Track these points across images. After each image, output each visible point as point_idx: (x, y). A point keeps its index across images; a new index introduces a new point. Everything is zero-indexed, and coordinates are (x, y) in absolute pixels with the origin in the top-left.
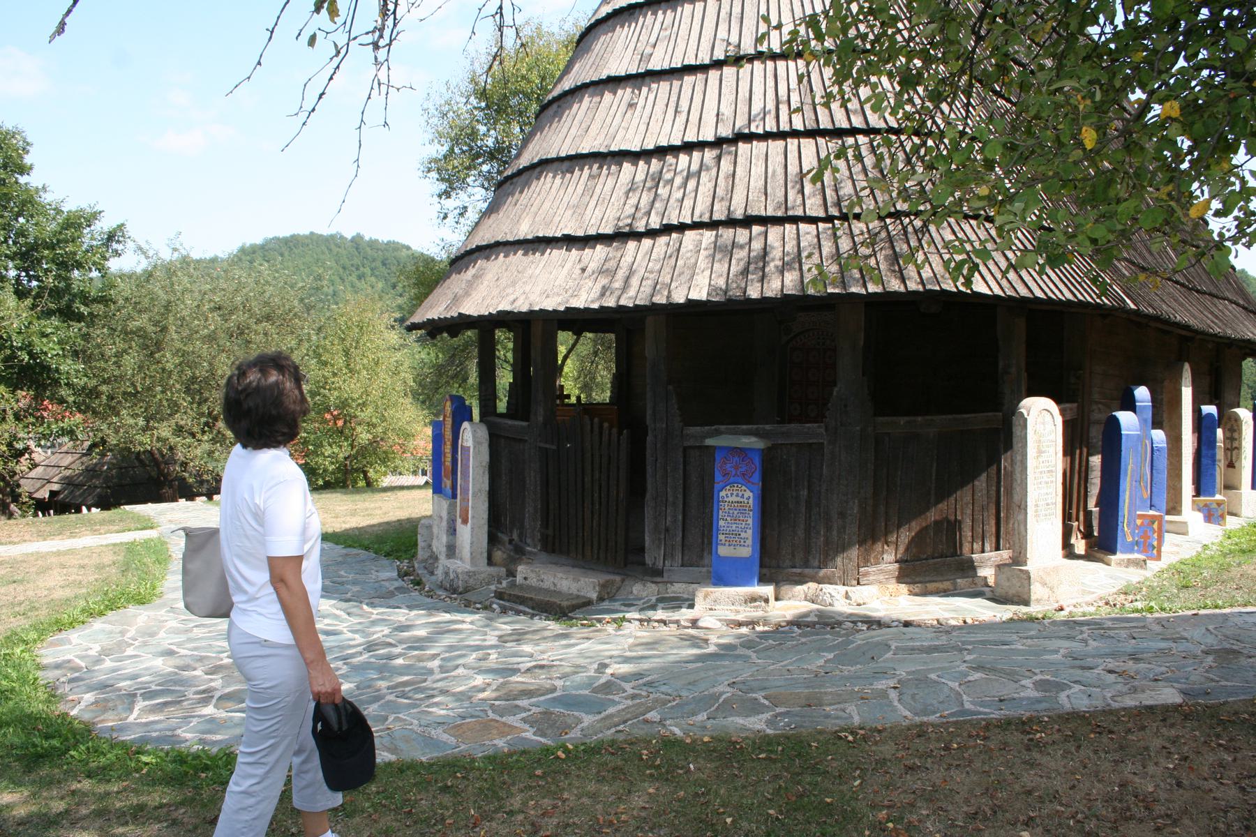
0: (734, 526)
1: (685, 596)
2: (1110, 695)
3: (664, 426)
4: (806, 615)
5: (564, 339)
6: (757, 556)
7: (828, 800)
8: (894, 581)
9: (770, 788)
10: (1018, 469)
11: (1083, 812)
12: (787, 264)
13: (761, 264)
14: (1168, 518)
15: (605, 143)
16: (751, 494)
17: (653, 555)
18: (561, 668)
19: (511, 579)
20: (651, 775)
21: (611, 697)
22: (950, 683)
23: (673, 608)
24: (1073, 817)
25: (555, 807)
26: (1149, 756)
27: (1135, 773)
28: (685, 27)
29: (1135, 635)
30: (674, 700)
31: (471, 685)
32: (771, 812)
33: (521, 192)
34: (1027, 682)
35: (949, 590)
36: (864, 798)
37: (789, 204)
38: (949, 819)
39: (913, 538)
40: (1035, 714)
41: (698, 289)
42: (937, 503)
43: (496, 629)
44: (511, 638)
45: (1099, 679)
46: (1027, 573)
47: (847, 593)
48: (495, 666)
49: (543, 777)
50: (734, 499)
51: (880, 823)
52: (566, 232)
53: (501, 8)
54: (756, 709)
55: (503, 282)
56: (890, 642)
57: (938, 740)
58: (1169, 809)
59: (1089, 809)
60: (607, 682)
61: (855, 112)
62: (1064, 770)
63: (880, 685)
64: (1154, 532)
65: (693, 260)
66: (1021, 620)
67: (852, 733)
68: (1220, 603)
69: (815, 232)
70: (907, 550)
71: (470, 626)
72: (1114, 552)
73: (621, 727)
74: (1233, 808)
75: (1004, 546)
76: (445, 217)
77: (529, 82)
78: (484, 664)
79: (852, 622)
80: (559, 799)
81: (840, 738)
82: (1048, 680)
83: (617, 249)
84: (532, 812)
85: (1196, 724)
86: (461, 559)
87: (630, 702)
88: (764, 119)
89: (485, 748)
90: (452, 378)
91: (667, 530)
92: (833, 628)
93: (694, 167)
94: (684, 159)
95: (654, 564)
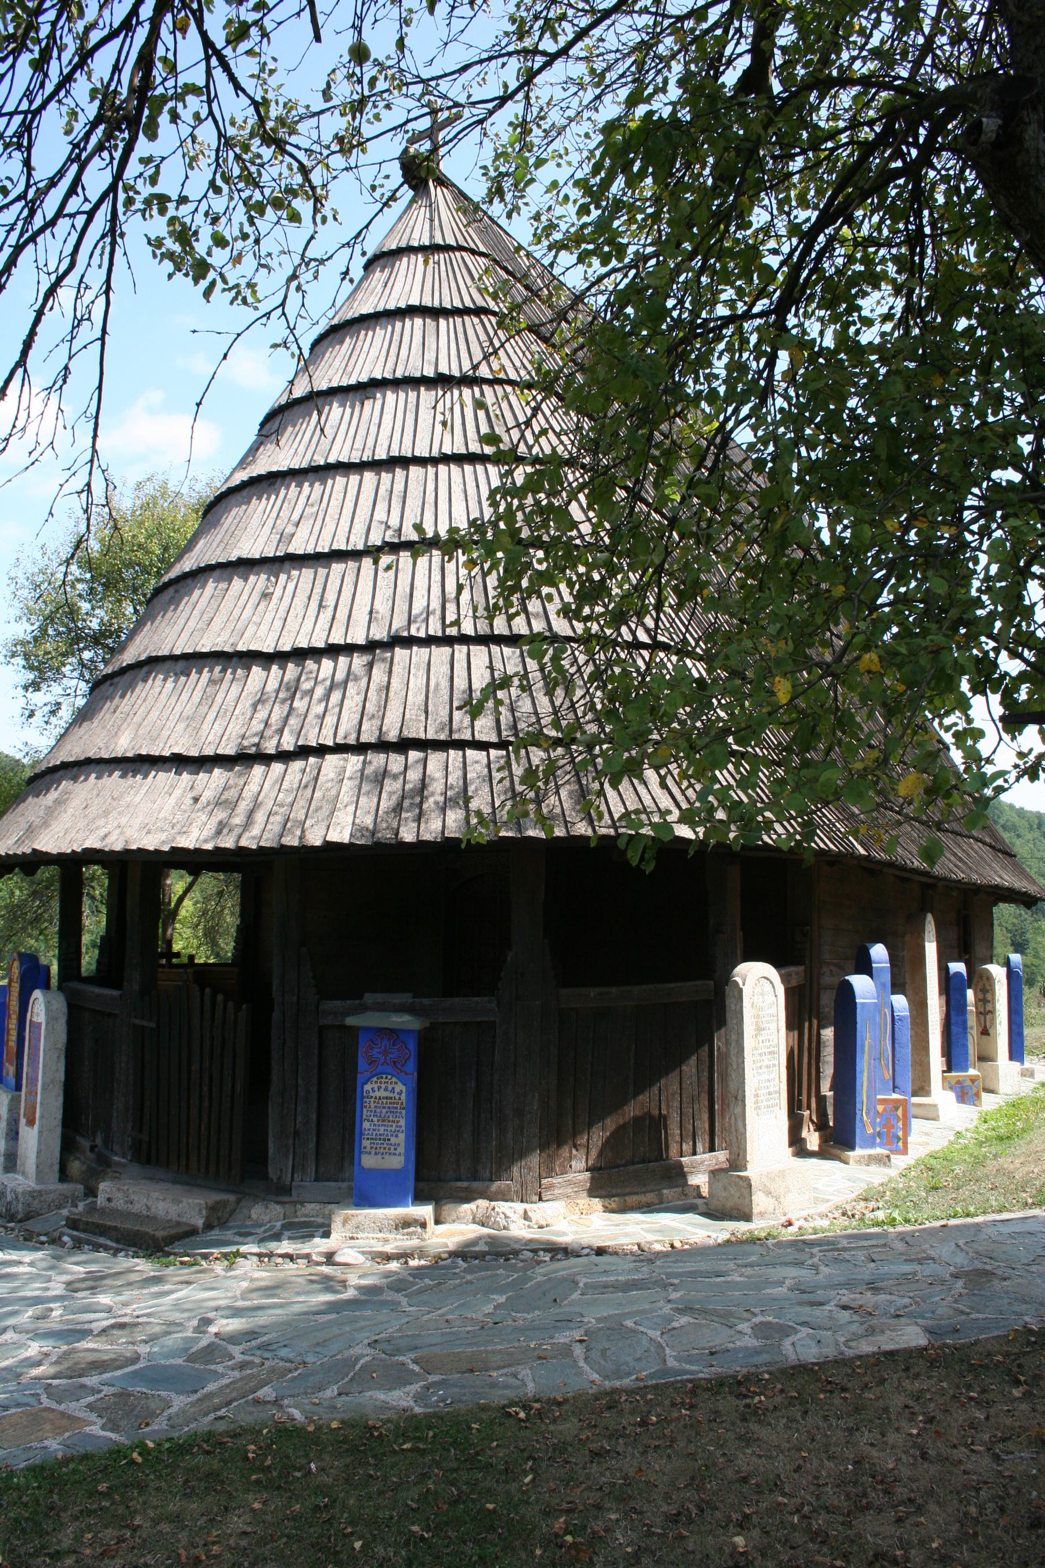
0: (382, 1129)
1: (320, 1220)
2: (843, 1339)
3: (295, 999)
4: (474, 1242)
5: (176, 883)
6: (412, 1168)
7: (490, 1506)
8: (585, 1194)
9: (415, 1492)
10: (733, 1051)
11: (810, 1504)
12: (451, 800)
13: (418, 800)
14: (915, 1100)
15: (231, 641)
16: (404, 1088)
17: (278, 1166)
18: (148, 1328)
19: (91, 1199)
20: (258, 1482)
21: (213, 1367)
22: (649, 1332)
23: (303, 1237)
24: (798, 1511)
25: (121, 1540)
26: (889, 1419)
27: (872, 1445)
28: (333, 510)
29: (874, 1257)
30: (296, 1369)
31: (22, 1357)
32: (415, 1528)
33: (123, 696)
34: (744, 1327)
35: (654, 1204)
36: (537, 1500)
37: (455, 726)
38: (645, 1525)
39: (608, 1139)
40: (753, 1370)
41: (339, 829)
42: (634, 1097)
43: (65, 1272)
44: (84, 1285)
45: (831, 1318)
46: (747, 1180)
47: (525, 1212)
48: (57, 1327)
49: (106, 1495)
50: (382, 1093)
51: (557, 1535)
52: (176, 751)
53: (88, 485)
54: (400, 1377)
55: (93, 811)
56: (578, 1278)
57: (633, 1412)
58: (912, 1491)
59: (818, 1498)
60: (209, 1346)
61: (536, 616)
62: (787, 1445)
63: (562, 1338)
64: (898, 1119)
65: (334, 792)
66: (741, 1242)
67: (525, 1407)
68: (972, 1209)
69: (485, 761)
70: (601, 1154)
71: (28, 1269)
72: (852, 1148)
73: (222, 1412)
74: (986, 1483)
75: (720, 1145)
76: (32, 715)
77: (148, 552)
78: (44, 1325)
79: (532, 1251)
80: (127, 1526)
81: (509, 1415)
82: (769, 1323)
83: (240, 775)
84: (88, 1551)
85: (943, 1372)
86: (23, 1173)
87: (237, 1374)
88: (427, 620)
89: (31, 1454)
90: (31, 923)
91: (296, 1133)
92: (507, 1260)
93: (340, 676)
94: (327, 664)
95: (279, 1178)
